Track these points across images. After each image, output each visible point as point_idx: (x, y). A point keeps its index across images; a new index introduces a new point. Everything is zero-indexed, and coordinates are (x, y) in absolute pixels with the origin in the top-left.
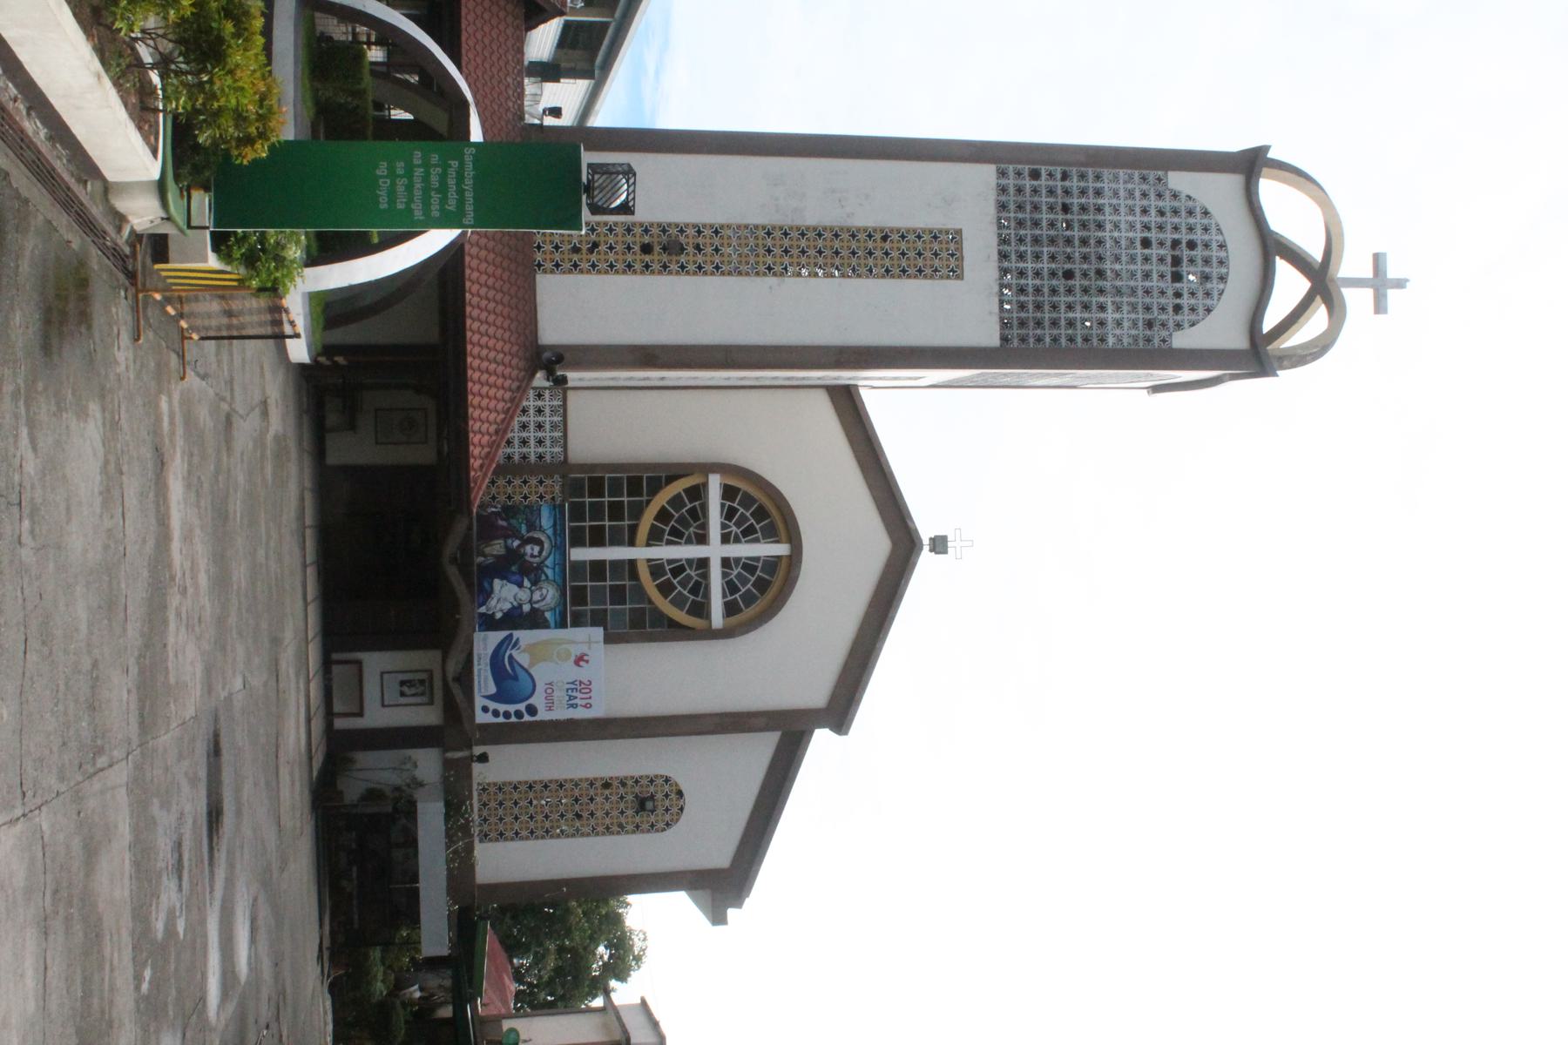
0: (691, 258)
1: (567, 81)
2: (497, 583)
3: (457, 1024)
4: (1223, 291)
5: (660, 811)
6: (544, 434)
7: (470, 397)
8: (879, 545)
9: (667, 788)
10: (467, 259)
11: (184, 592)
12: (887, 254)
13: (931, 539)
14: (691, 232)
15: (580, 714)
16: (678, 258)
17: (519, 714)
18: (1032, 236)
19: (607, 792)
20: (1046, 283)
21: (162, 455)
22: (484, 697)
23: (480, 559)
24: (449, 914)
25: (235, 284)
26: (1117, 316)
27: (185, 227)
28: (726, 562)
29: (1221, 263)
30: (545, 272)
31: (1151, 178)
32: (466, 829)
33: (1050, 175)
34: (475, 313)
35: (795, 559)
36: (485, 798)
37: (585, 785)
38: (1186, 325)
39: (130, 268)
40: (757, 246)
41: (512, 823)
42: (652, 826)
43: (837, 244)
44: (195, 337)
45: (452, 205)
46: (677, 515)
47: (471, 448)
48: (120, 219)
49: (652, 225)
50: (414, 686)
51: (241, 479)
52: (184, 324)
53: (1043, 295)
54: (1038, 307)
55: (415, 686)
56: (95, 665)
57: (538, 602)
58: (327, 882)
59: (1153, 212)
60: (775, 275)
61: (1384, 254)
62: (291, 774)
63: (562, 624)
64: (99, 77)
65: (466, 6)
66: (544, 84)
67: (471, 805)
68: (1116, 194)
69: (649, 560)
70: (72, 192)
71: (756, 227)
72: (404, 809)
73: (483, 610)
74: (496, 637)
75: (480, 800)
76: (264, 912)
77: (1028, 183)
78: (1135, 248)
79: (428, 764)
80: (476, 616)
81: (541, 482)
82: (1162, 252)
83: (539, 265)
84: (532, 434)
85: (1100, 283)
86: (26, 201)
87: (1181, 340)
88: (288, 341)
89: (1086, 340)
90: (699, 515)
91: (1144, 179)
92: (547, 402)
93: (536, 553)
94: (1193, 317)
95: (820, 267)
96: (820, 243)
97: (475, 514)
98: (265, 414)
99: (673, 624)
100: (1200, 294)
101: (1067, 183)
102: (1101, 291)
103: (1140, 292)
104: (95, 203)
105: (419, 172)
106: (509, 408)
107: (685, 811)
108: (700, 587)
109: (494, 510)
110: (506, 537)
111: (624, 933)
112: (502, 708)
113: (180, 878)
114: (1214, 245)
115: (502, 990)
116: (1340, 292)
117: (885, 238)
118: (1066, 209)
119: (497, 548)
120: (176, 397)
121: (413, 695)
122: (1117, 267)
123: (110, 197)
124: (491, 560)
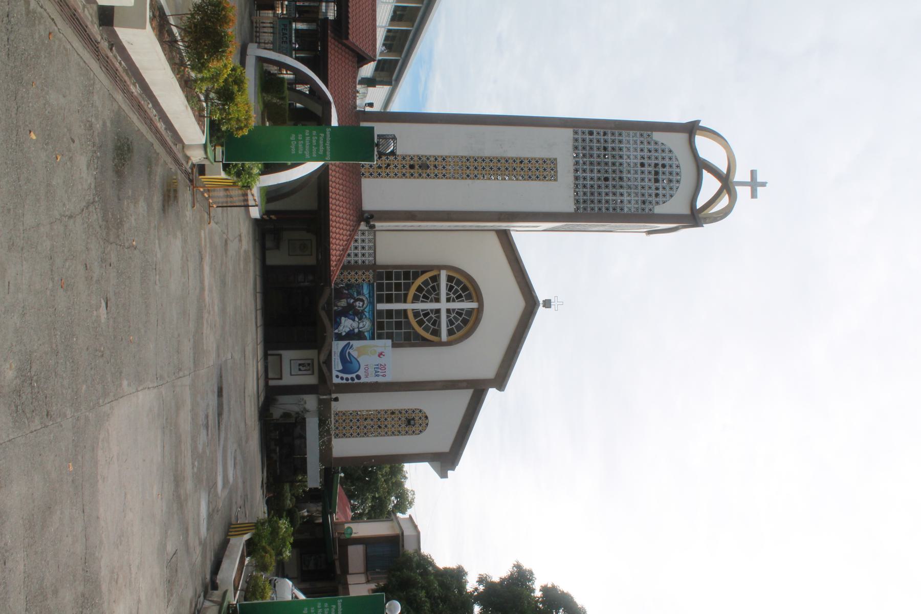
0: (432, 171)
1: (379, 86)
2: (343, 319)
3: (325, 524)
4: (678, 187)
5: (417, 425)
6: (365, 251)
7: (331, 234)
8: (520, 304)
10: (330, 172)
11: (209, 313)
12: (522, 169)
13: (543, 301)
14: (432, 159)
15: (380, 379)
16: (426, 171)
17: (352, 379)
18: (590, 161)
19: (393, 416)
20: (596, 183)
21: (202, 255)
22: (338, 371)
23: (336, 308)
24: (320, 471)
25: (232, 184)
26: (629, 198)
27: (213, 161)
28: (448, 311)
29: (677, 174)
30: (365, 177)
31: (645, 135)
32: (328, 431)
33: (598, 133)
34: (334, 196)
35: (480, 310)
37: (383, 413)
38: (661, 203)
39: (191, 178)
40: (462, 165)
41: (349, 430)
42: (414, 432)
43: (499, 165)
44: (215, 206)
45: (321, 152)
46: (426, 289)
47: (331, 257)
48: (188, 158)
49: (414, 156)
50: (305, 366)
51: (231, 268)
52: (211, 201)
53: (594, 189)
54: (592, 194)
55: (305, 366)
56: (179, 335)
57: (361, 328)
58: (265, 455)
59: (646, 150)
60: (470, 179)
61: (756, 171)
62: (251, 401)
63: (373, 338)
64: (186, 107)
65: (330, 53)
66: (368, 88)
67: (331, 421)
68: (628, 142)
69: (413, 310)
70: (172, 149)
71: (462, 157)
72: (300, 422)
73: (336, 331)
74: (342, 344)
75: (335, 419)
76: (239, 458)
77: (588, 137)
78: (637, 167)
79: (311, 402)
80: (334, 334)
81: (364, 273)
82: (650, 169)
83: (363, 174)
84: (359, 251)
85: (621, 183)
86: (158, 154)
87: (658, 210)
88: (250, 208)
89: (614, 209)
90: (436, 289)
91: (641, 135)
92: (367, 237)
93: (361, 306)
94: (664, 199)
95: (507, 176)
96: (491, 164)
97: (333, 287)
98: (240, 240)
99: (424, 339)
100: (668, 188)
101: (606, 137)
102: (621, 187)
103: (639, 188)
104: (179, 153)
105: (308, 138)
106: (349, 239)
107: (429, 425)
108: (437, 322)
109: (342, 285)
110: (347, 298)
111: (404, 491)
112: (345, 376)
113: (208, 431)
114: (674, 166)
115: (345, 513)
116: (735, 188)
117: (521, 162)
118: (605, 149)
119: (343, 303)
120: (207, 231)
122: (629, 176)
123: (185, 150)
124: (340, 308)
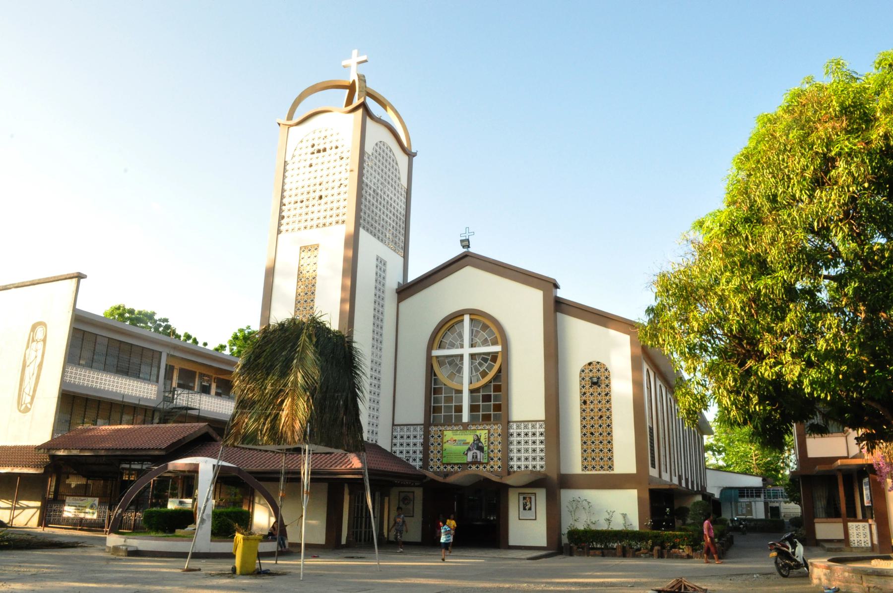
8: (468, 272)
9: (587, 371)
35: (473, 313)
36: (590, 467)
99: (500, 371)
121: (531, 503)
